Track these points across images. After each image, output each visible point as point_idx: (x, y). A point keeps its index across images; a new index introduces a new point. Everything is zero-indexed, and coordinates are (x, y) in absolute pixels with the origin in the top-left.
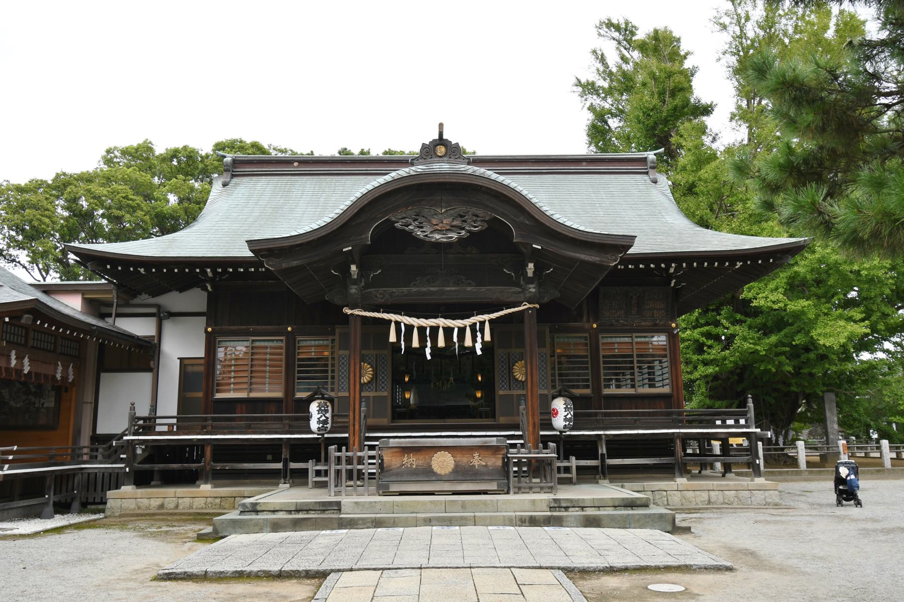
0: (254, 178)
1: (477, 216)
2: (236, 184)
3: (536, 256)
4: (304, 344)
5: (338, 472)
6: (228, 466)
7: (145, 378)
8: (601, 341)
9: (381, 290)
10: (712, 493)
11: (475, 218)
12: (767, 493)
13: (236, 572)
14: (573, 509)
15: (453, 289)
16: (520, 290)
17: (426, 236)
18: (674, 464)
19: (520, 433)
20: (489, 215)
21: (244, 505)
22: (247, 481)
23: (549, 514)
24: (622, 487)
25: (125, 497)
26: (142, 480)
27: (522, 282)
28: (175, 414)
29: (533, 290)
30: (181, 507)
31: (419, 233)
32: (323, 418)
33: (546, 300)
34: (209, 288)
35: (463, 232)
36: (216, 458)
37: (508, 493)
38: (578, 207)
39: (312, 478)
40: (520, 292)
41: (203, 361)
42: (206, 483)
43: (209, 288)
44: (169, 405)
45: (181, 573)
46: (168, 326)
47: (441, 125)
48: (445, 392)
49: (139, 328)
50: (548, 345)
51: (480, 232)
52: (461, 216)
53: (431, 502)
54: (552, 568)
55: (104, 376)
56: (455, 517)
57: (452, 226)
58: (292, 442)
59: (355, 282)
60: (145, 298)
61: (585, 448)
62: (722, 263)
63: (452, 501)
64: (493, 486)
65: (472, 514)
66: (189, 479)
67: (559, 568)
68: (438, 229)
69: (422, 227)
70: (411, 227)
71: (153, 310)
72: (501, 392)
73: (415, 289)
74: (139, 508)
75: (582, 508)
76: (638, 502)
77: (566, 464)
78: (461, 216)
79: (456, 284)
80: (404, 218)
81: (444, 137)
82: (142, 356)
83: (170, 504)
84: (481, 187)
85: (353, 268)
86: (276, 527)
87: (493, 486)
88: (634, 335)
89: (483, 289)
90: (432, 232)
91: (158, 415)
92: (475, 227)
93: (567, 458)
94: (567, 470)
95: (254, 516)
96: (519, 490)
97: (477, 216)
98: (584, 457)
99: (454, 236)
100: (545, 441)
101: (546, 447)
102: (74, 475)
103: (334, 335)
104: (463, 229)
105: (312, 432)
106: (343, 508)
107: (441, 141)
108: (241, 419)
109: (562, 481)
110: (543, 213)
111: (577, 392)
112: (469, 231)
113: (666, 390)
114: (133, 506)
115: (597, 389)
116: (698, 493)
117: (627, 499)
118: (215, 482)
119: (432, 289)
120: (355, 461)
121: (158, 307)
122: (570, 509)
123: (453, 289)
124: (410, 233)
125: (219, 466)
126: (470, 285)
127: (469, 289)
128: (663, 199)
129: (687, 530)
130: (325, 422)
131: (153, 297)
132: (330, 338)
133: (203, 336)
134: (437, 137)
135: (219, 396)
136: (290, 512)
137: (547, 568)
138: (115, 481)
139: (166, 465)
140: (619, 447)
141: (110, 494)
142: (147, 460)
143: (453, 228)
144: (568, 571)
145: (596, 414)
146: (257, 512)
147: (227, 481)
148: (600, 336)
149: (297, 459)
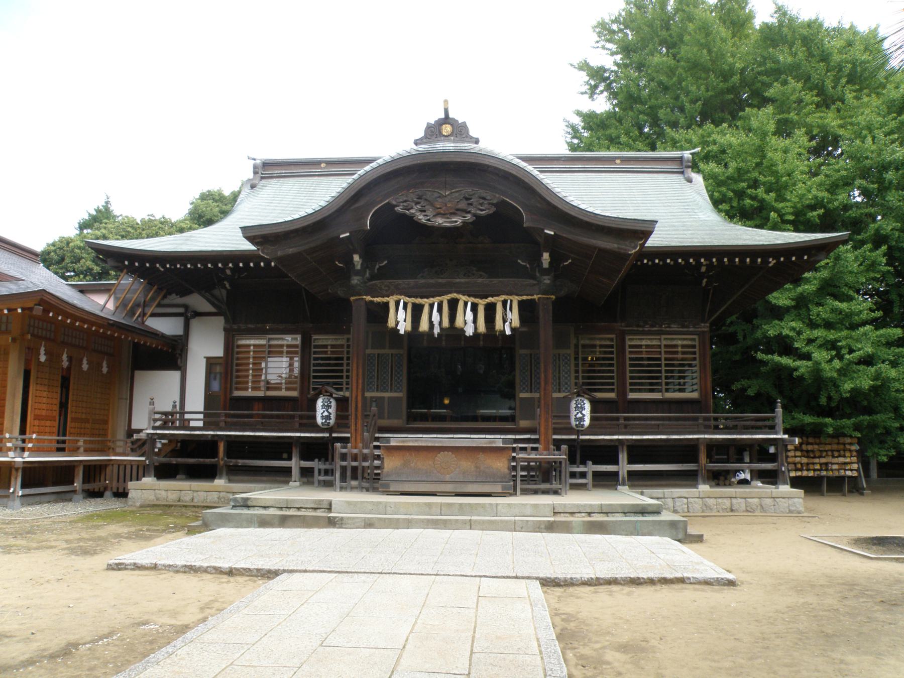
0: (282, 180)
1: (484, 199)
2: (264, 186)
3: (553, 244)
4: (320, 343)
5: (344, 469)
6: (241, 462)
7: (176, 375)
8: (628, 343)
9: (387, 282)
10: (734, 501)
11: (481, 201)
12: (791, 501)
13: (186, 566)
14: (579, 515)
15: (463, 280)
16: (535, 282)
17: (429, 220)
18: (696, 471)
19: (537, 437)
20: (497, 197)
21: (235, 500)
22: (264, 478)
23: (552, 519)
24: (642, 494)
25: (146, 489)
26: (165, 472)
27: (538, 274)
28: (202, 409)
29: (547, 282)
30: (195, 500)
31: (421, 218)
32: (326, 414)
33: (563, 293)
34: (227, 286)
35: (469, 216)
36: (229, 454)
37: (514, 494)
38: (602, 194)
39: (317, 477)
40: (535, 285)
41: (221, 361)
42: (220, 478)
43: (227, 286)
44: (196, 401)
45: (130, 565)
46: (195, 323)
47: (446, 102)
48: (453, 388)
49: (167, 326)
50: (572, 346)
51: (489, 216)
52: (467, 199)
53: (426, 504)
54: (528, 578)
55: (138, 374)
56: (450, 520)
57: (458, 210)
58: (302, 441)
59: (358, 273)
60: (174, 299)
61: (607, 453)
62: (800, 257)
63: (448, 504)
64: (498, 488)
65: (469, 518)
66: (207, 473)
67: (537, 578)
68: (439, 213)
69: (424, 211)
70: (412, 211)
71: (181, 310)
72: (523, 395)
73: (422, 281)
74: (158, 499)
75: (589, 514)
76: (650, 509)
77: (582, 469)
78: (467, 199)
79: (466, 275)
80: (405, 201)
81: (451, 116)
82: (169, 355)
83: (187, 497)
84: (488, 166)
85: (356, 258)
86: (264, 523)
87: (498, 488)
88: (663, 337)
89: (495, 281)
90: (435, 216)
91: (186, 410)
92: (482, 210)
93: (583, 463)
94: (583, 475)
95: (245, 511)
96: (525, 492)
97: (484, 199)
98: (592, 460)
99: (458, 220)
100: (558, 444)
101: (558, 449)
102: (106, 466)
103: (349, 333)
104: (469, 212)
105: (315, 427)
106: (333, 506)
107: (447, 120)
108: (258, 416)
109: (574, 487)
110: (555, 195)
111: (599, 395)
112: (474, 215)
113: (695, 395)
114: (152, 497)
115: (622, 393)
116: (720, 500)
117: (638, 505)
118: (232, 477)
119: (440, 280)
120: (349, 458)
121: (186, 307)
122: (577, 515)
123: (463, 280)
124: (410, 219)
125: (232, 462)
126: (481, 276)
127: (480, 280)
128: (698, 198)
129: (699, 539)
130: (328, 417)
131: (181, 297)
132: (346, 336)
133: (223, 334)
134: (443, 116)
135: (237, 394)
136: (281, 508)
137: (523, 578)
138: (139, 471)
139: (189, 458)
140: (638, 453)
141: (131, 485)
142: (175, 453)
143: (457, 212)
144: (547, 583)
145: (617, 419)
146: (248, 507)
147: (246, 478)
148: (627, 338)
149: (319, 458)
